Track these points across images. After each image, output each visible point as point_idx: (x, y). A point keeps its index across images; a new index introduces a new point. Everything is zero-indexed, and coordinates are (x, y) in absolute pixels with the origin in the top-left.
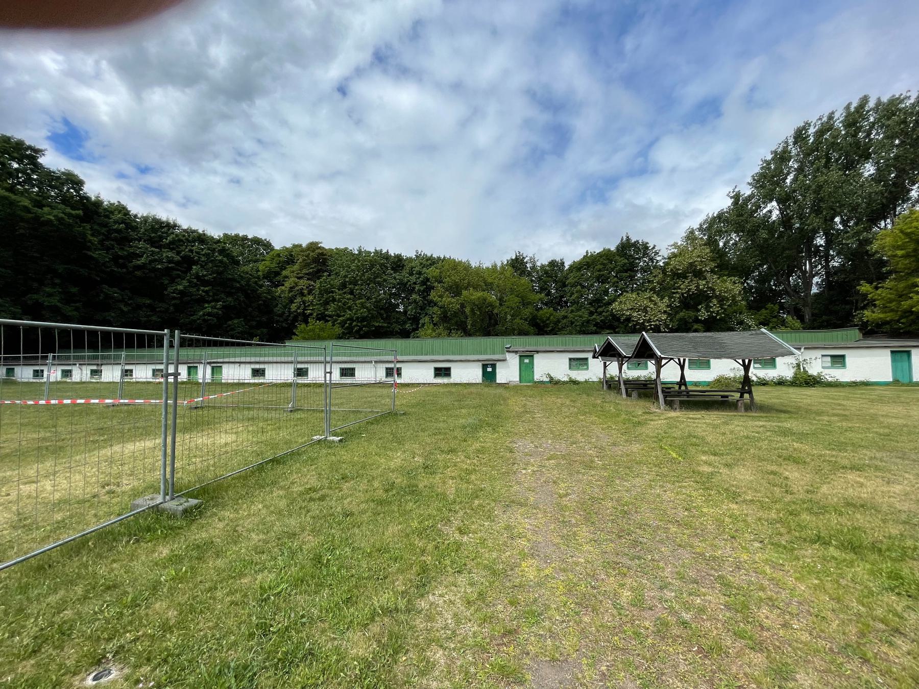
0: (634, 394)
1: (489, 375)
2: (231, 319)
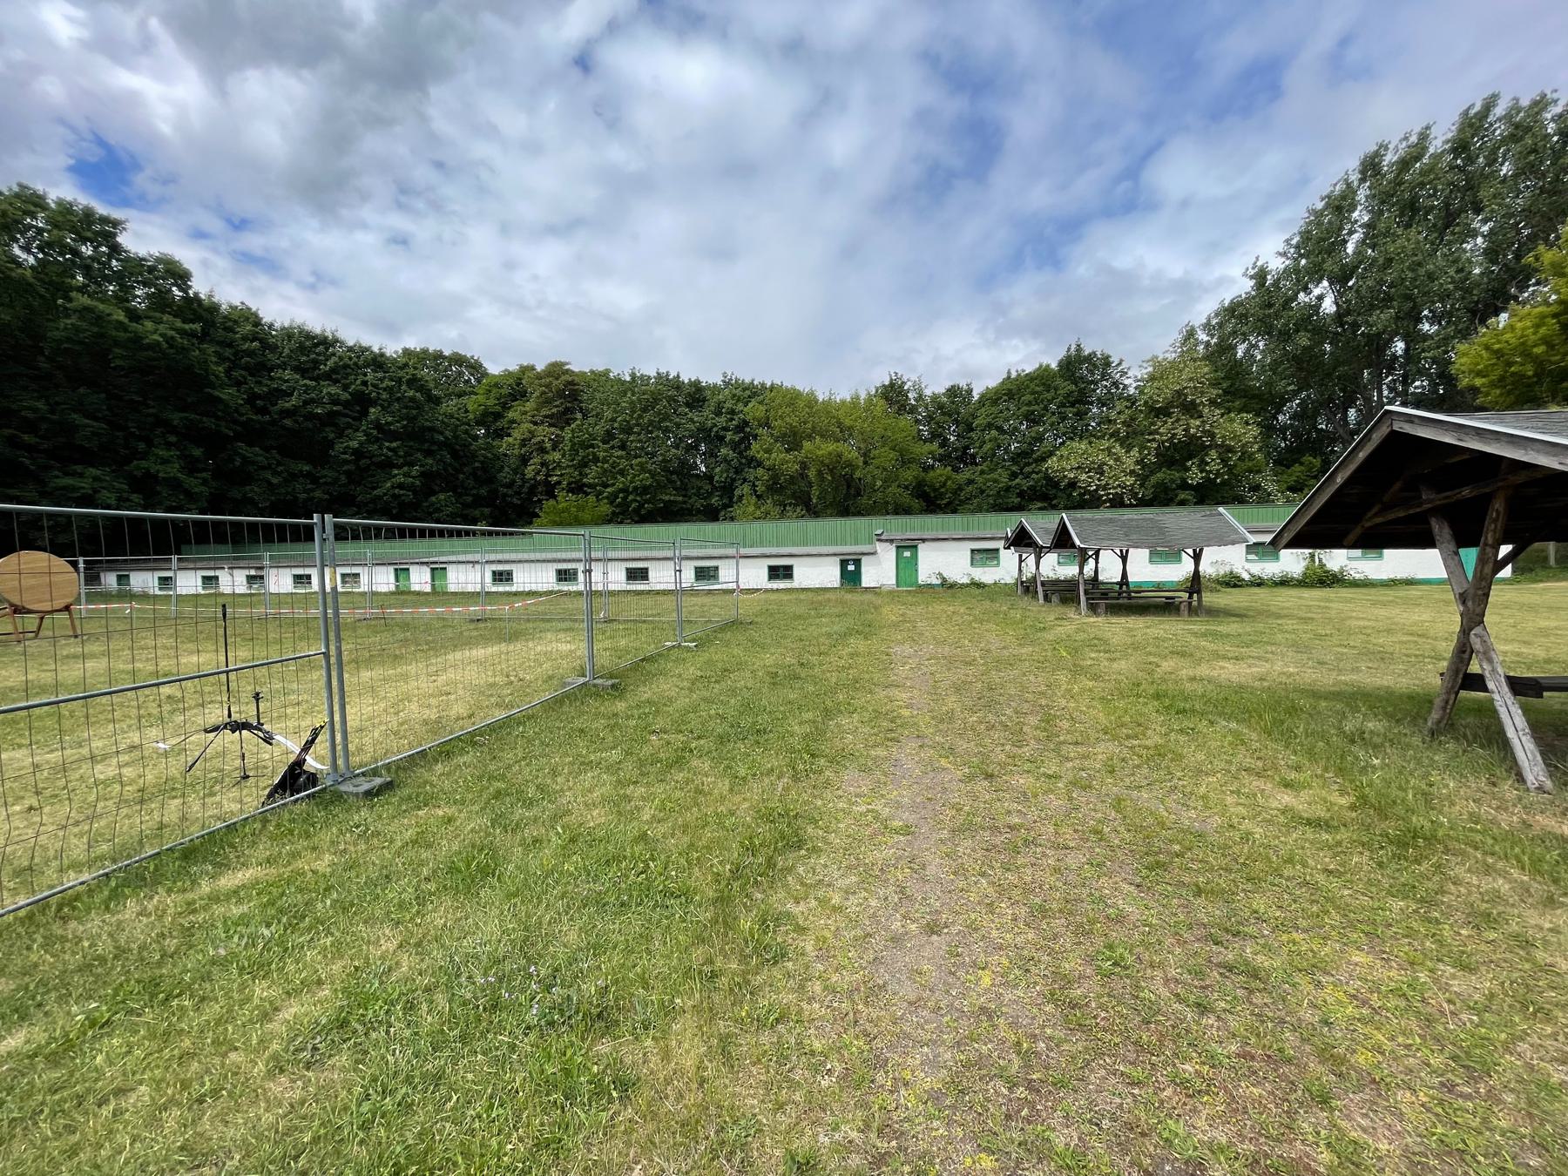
0: (1055, 598)
1: (851, 575)
2: (434, 493)
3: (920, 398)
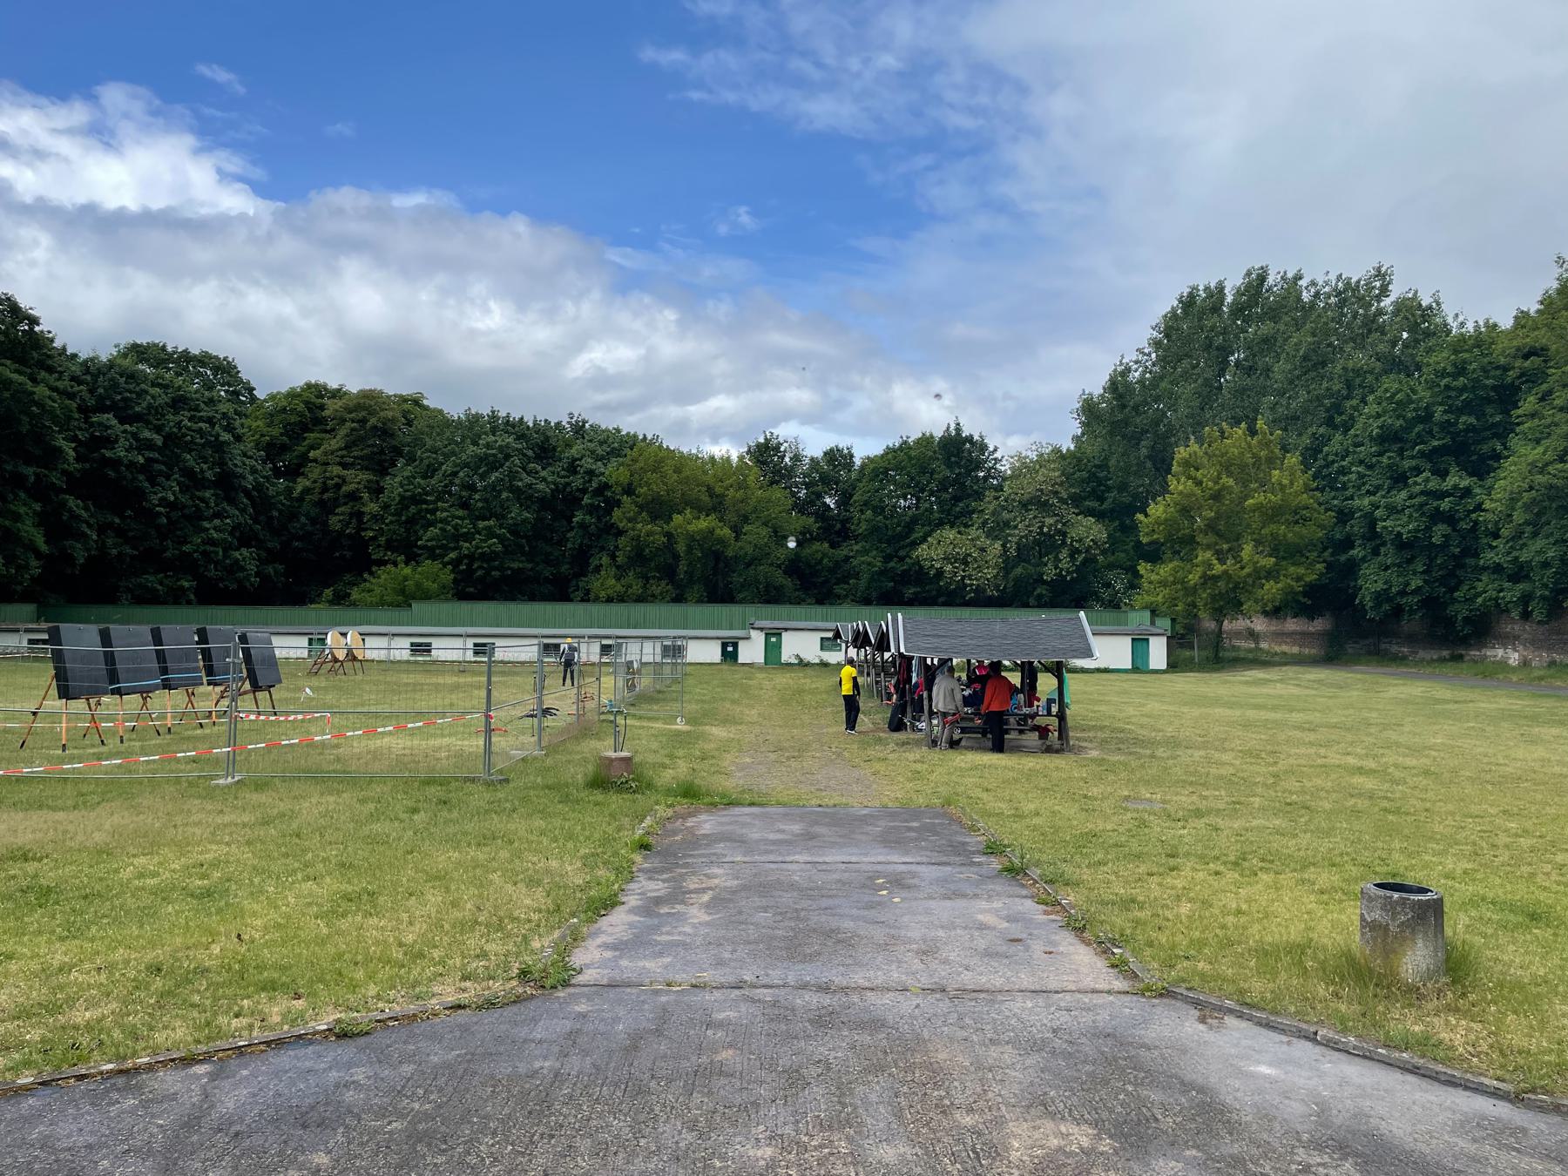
1: (730, 653)
3: (797, 458)
